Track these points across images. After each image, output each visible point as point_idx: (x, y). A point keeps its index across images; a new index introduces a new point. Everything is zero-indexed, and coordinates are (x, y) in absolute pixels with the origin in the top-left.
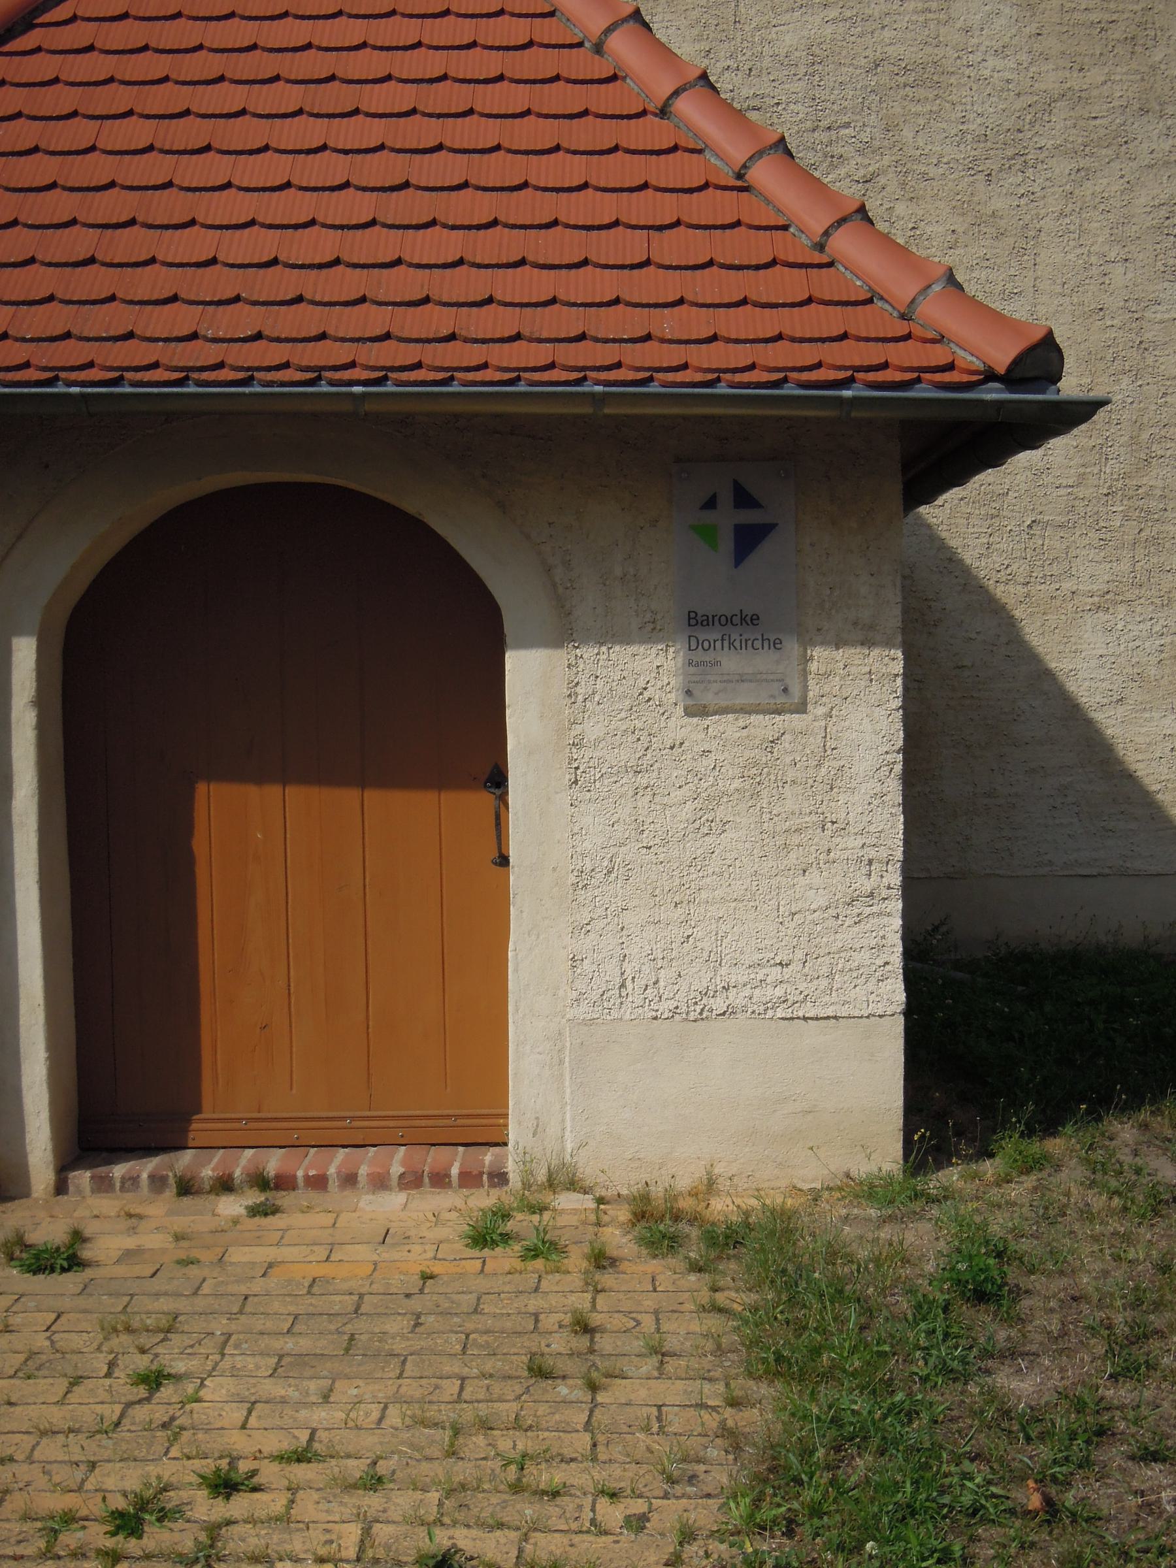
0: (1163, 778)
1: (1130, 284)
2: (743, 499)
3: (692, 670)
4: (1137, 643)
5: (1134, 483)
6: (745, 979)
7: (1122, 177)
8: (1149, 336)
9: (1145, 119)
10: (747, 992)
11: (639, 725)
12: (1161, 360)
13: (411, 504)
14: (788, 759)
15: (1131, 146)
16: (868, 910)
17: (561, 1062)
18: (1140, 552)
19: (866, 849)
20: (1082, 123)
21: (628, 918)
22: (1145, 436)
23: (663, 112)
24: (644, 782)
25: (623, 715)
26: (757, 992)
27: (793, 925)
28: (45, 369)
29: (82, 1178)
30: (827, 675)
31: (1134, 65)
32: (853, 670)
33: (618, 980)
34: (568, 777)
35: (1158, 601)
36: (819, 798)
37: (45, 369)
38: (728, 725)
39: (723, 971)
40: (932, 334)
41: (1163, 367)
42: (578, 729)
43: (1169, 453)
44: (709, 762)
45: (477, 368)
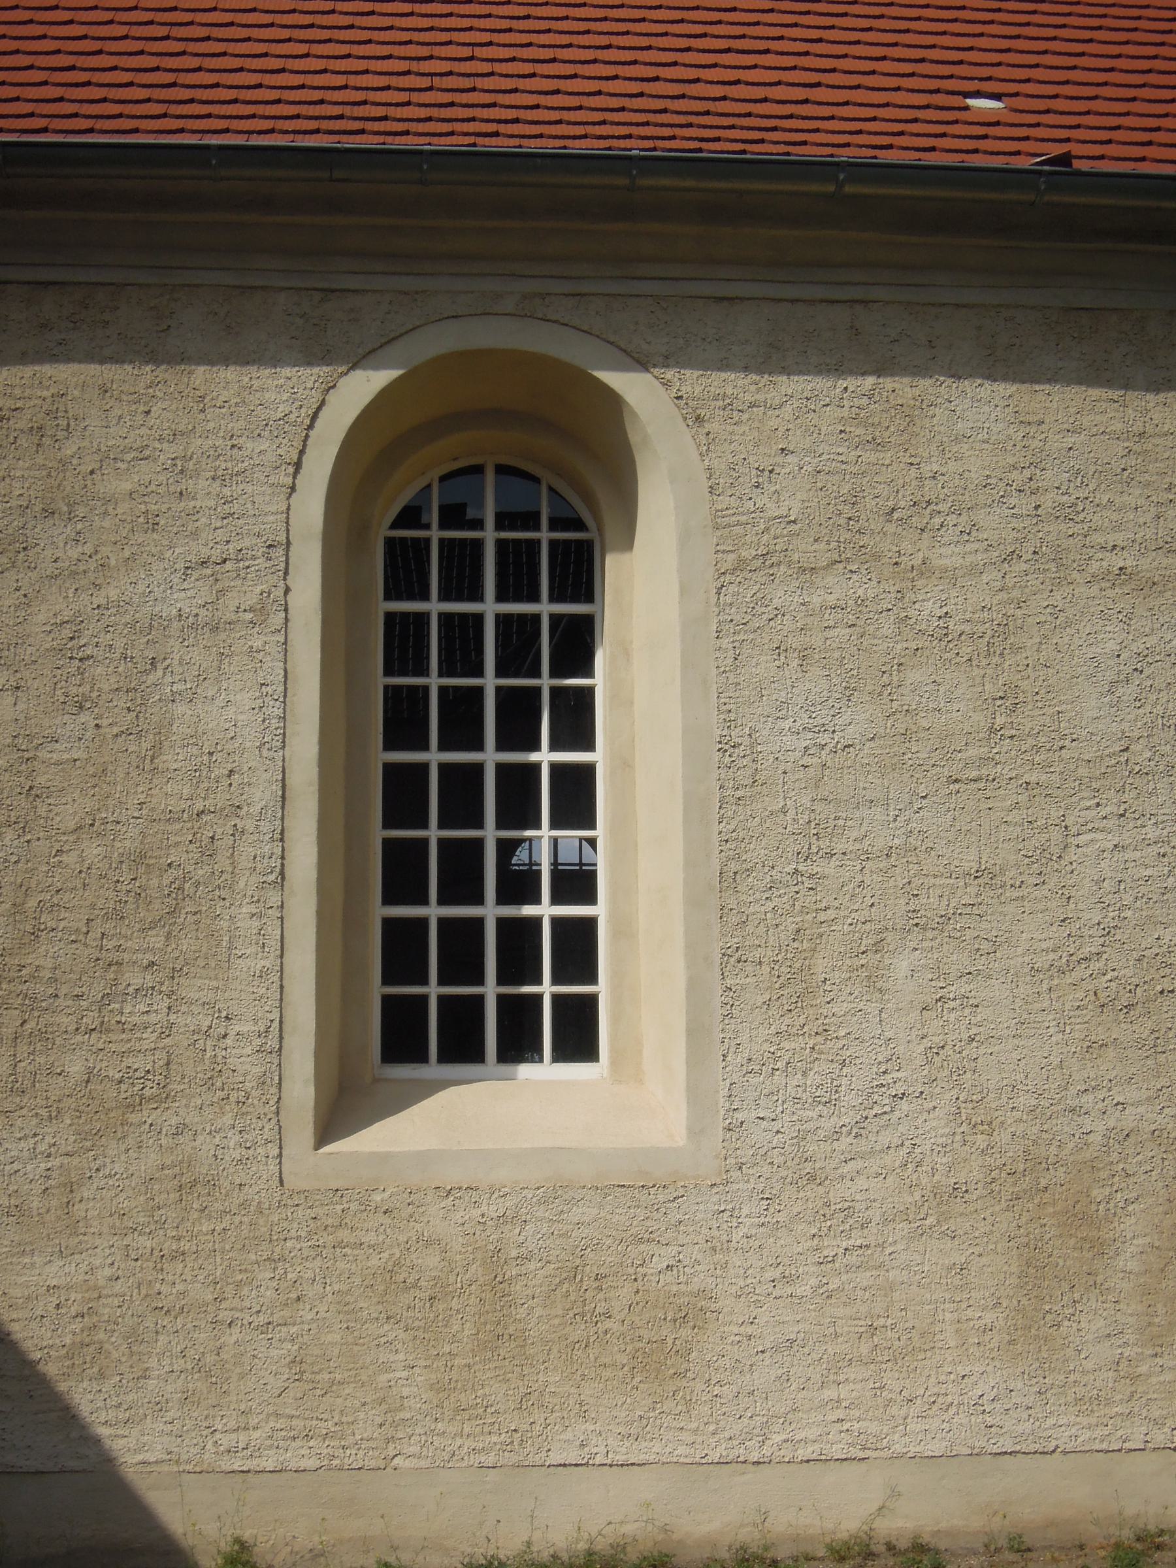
0: (45, 1344)
1: (22, 717)
4: (15, 1166)
5: (16, 962)
7: (17, 589)
8: (41, 780)
12: (56, 810)
13: (613, 379)
15: (30, 553)
18: (23, 1049)
22: (32, 903)
31: (40, 460)
35: (44, 1113)
41: (58, 819)
43: (62, 925)
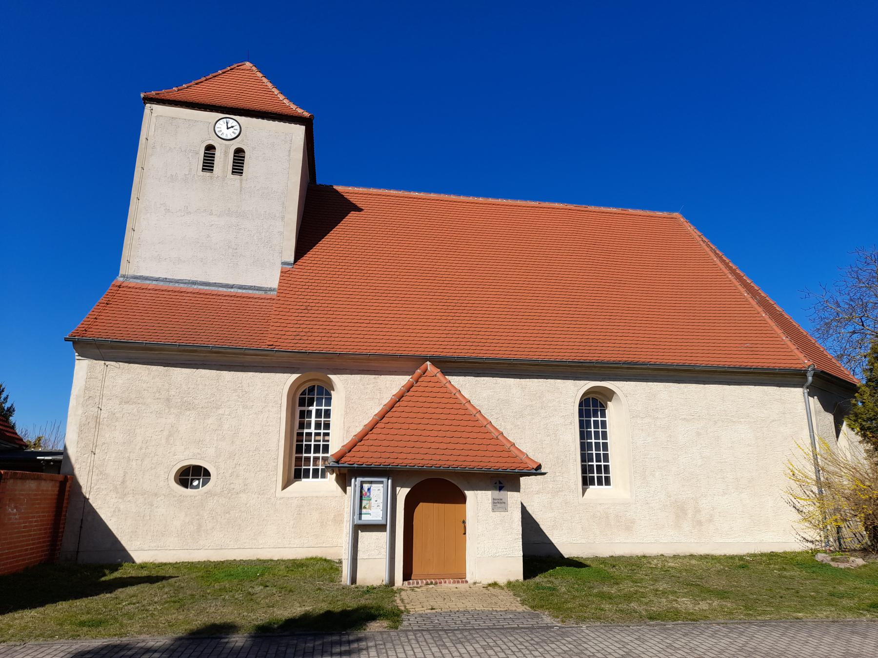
2: (500, 483)
29: (406, 582)
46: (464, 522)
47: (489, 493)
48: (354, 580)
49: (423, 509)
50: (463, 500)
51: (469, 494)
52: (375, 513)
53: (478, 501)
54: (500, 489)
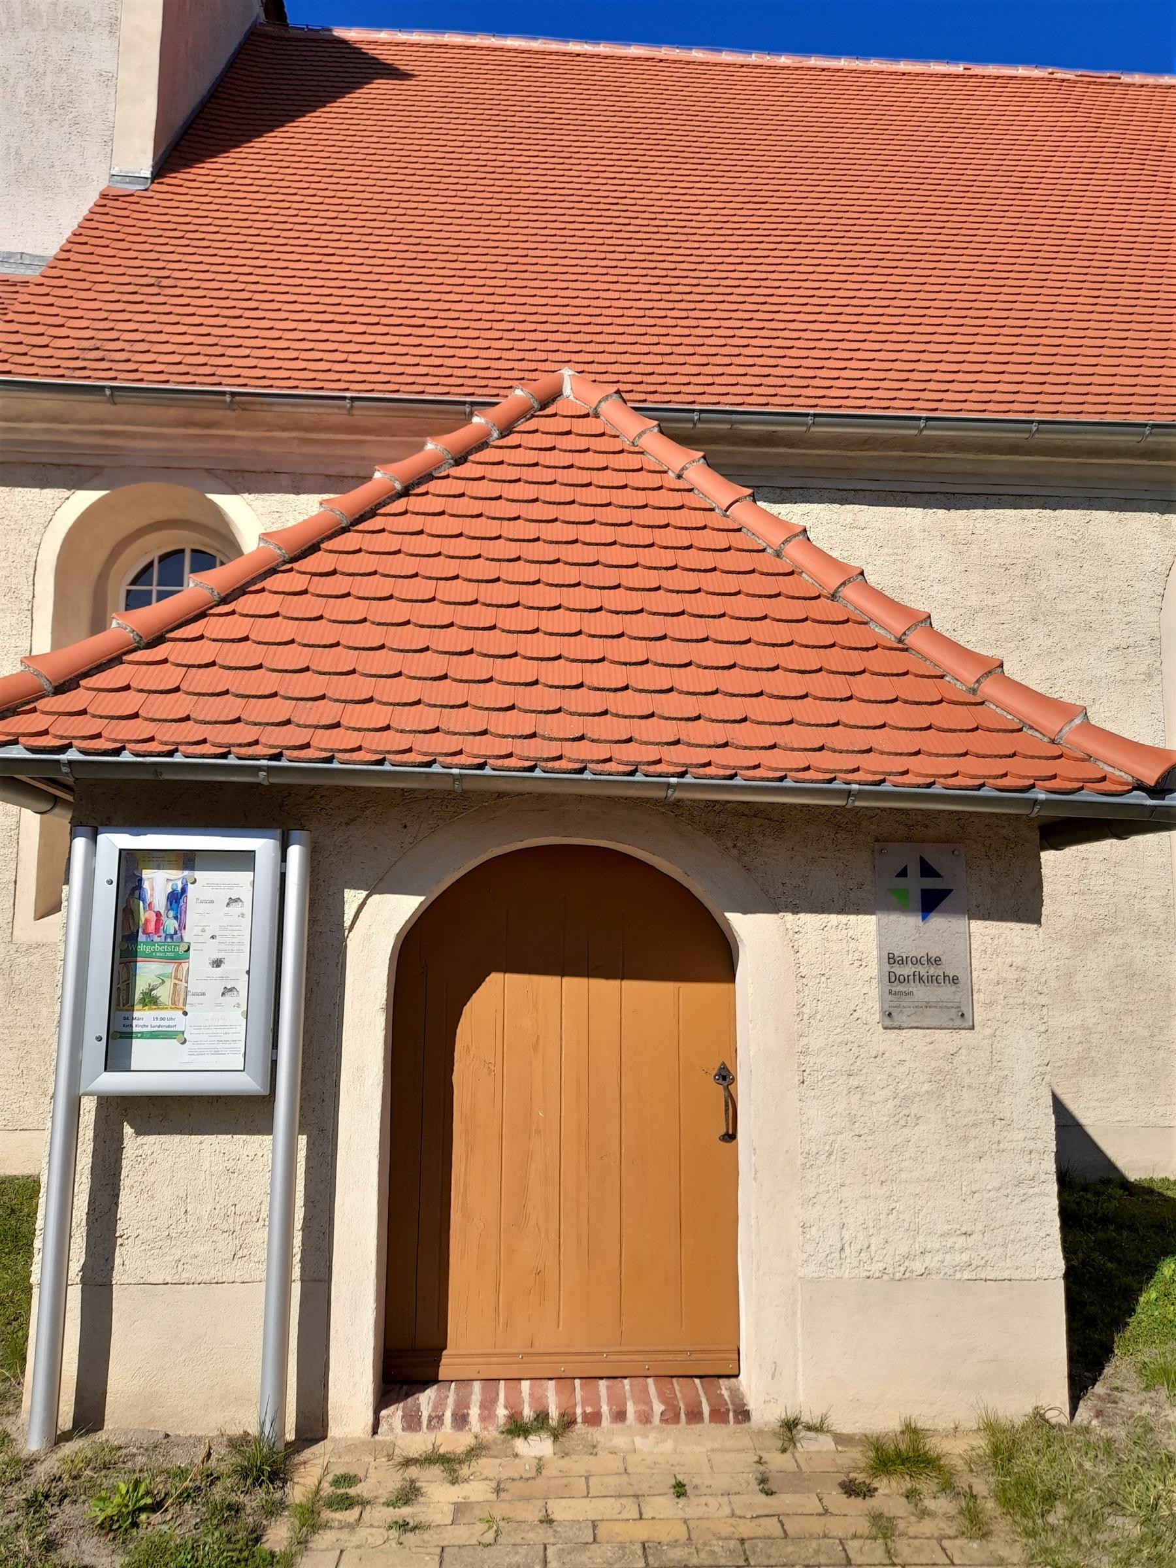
2: (927, 870)
3: (890, 997)
6: (938, 1246)
9: (1034, 625)
10: (940, 1257)
11: (851, 1038)
14: (965, 1069)
16: (1031, 1191)
17: (794, 1313)
19: (1027, 1142)
20: (995, 627)
21: (845, 1193)
23: (833, 597)
24: (856, 1083)
25: (838, 1030)
26: (948, 1257)
27: (973, 1202)
28: (425, 754)
29: (394, 1414)
30: (991, 1004)
32: (1011, 1001)
33: (839, 1245)
34: (797, 1078)
36: (990, 1100)
37: (425, 754)
38: (915, 1038)
39: (921, 1238)
40: (1081, 755)
42: (804, 1041)
44: (902, 1069)
45: (250, 744)
46: (725, 1076)
47: (865, 926)
48: (90, 1414)
49: (512, 1017)
50: (718, 959)
51: (753, 931)
52: (205, 1036)
53: (801, 967)
54: (930, 903)
